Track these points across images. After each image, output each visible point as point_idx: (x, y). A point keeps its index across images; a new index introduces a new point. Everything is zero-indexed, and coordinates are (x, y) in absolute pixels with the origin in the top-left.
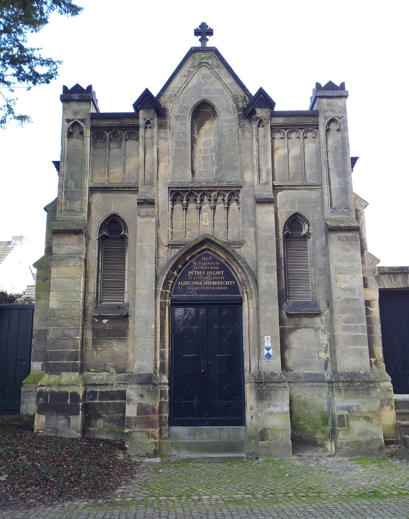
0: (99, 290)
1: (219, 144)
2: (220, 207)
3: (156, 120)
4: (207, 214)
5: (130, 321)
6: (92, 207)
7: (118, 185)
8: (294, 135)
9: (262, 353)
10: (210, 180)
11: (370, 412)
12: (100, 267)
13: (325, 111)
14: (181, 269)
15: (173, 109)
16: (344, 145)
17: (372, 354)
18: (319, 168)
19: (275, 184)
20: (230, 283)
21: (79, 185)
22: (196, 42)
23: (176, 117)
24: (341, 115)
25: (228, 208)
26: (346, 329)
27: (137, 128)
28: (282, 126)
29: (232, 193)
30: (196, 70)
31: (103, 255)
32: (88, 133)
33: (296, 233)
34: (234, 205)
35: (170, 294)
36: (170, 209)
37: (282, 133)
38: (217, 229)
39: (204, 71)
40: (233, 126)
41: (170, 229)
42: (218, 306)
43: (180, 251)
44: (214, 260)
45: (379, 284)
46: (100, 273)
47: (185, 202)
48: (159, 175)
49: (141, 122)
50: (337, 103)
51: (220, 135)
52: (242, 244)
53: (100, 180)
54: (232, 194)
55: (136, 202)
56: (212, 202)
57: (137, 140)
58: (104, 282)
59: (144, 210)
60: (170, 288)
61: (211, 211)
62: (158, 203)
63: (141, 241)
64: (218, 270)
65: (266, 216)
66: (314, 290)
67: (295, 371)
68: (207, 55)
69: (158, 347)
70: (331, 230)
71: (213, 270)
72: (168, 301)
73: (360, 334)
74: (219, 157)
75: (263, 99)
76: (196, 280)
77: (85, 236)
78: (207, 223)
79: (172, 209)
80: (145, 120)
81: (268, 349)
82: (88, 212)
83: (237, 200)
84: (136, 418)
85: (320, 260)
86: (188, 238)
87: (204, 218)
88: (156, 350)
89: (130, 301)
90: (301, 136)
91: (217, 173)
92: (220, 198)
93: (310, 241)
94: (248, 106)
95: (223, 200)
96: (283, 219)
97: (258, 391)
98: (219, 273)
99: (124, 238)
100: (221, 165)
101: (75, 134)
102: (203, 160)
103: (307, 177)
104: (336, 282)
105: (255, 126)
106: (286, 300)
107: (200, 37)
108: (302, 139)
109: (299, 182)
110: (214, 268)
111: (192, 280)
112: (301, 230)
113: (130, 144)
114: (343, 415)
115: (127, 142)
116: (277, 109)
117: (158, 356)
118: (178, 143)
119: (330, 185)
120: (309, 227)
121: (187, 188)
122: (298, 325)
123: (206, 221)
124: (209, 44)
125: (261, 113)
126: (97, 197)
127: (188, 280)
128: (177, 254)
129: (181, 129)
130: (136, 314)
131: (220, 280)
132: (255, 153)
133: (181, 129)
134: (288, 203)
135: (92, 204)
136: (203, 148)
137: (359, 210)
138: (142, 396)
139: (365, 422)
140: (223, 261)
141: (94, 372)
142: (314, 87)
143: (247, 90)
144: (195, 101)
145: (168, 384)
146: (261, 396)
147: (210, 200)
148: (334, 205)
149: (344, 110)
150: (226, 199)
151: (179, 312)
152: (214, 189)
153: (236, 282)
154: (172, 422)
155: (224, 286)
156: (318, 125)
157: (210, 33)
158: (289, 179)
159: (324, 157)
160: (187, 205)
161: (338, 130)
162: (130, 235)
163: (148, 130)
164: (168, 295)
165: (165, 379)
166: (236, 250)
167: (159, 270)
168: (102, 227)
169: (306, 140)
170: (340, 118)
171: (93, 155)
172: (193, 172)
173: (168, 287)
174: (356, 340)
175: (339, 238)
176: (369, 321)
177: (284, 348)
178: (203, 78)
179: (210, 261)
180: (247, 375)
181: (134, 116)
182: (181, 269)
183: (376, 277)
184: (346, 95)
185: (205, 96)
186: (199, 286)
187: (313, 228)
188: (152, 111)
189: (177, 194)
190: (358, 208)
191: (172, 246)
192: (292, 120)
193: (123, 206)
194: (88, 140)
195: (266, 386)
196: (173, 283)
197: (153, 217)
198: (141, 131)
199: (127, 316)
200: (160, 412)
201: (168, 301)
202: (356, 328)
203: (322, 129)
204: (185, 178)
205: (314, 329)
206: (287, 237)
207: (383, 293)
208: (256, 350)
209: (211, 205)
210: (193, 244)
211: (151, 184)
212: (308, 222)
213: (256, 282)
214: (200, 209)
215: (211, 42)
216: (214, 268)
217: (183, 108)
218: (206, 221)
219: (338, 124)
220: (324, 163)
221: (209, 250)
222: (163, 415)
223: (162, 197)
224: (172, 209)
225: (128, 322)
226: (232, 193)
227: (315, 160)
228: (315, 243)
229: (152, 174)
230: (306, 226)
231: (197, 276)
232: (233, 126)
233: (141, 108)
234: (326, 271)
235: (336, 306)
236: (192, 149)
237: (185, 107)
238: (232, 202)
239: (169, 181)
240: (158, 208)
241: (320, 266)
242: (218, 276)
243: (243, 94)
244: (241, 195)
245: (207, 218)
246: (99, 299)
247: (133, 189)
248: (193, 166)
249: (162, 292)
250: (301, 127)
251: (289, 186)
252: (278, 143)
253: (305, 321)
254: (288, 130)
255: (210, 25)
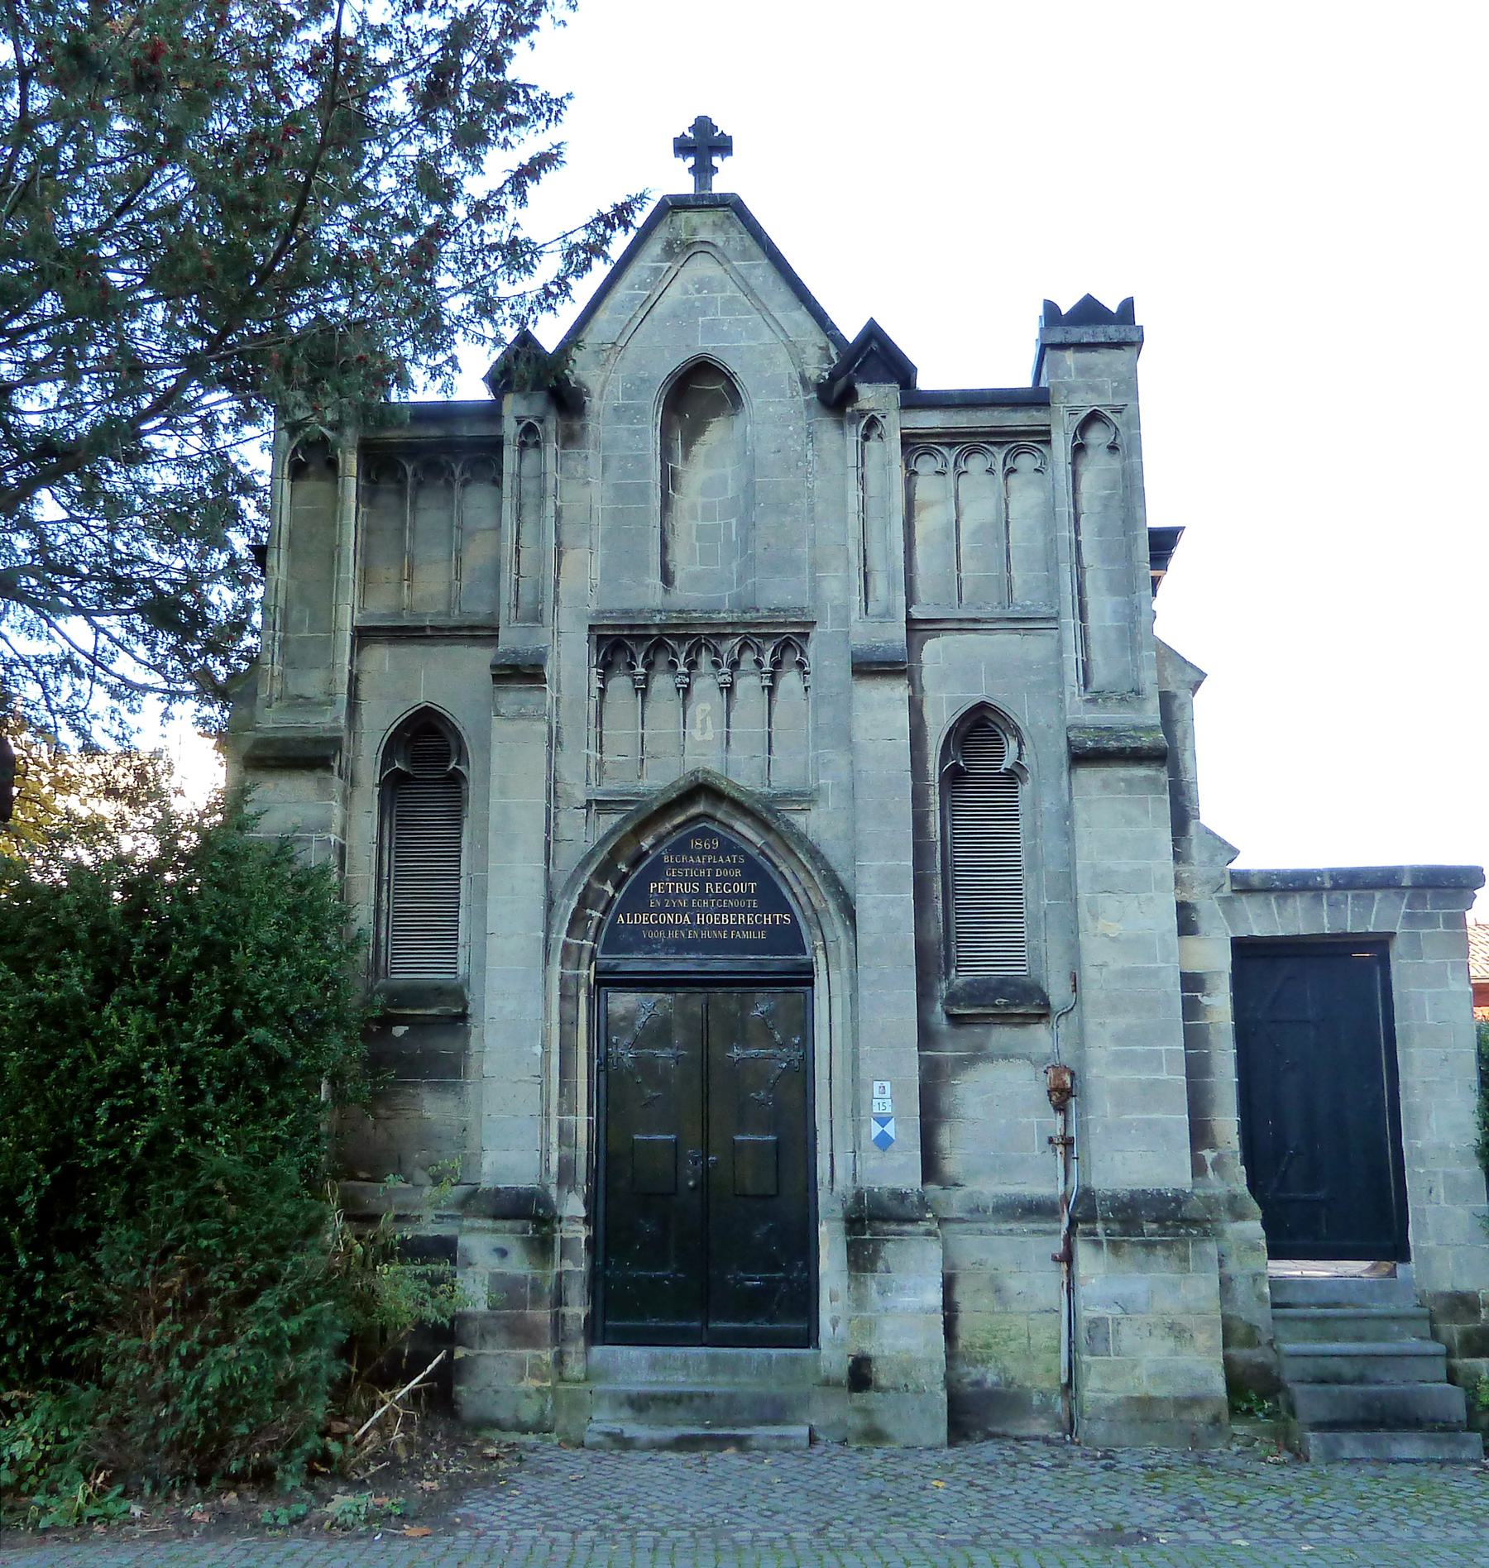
0: (383, 936)
1: (749, 489)
2: (749, 684)
3: (552, 425)
4: (708, 707)
5: (474, 1031)
7: (439, 622)
8: (976, 464)
9: (864, 1131)
10: (721, 599)
12: (386, 869)
13: (1071, 390)
14: (626, 876)
17: (1200, 1133)
18: (1051, 564)
19: (916, 616)
20: (774, 920)
21: (325, 621)
22: (679, 179)
23: (616, 409)
24: (1118, 402)
25: (771, 690)
28: (938, 435)
29: (783, 642)
30: (678, 266)
31: (394, 831)
32: (350, 463)
33: (981, 765)
34: (790, 680)
35: (593, 951)
36: (595, 693)
37: (939, 458)
39: (703, 267)
40: (791, 436)
41: (593, 753)
42: (740, 989)
43: (625, 820)
44: (728, 848)
45: (1233, 927)
46: (385, 887)
47: (641, 670)
48: (561, 589)
49: (510, 429)
51: (750, 464)
53: (381, 607)
54: (786, 645)
55: (487, 674)
56: (724, 669)
57: (497, 483)
59: (512, 698)
60: (591, 933)
61: (720, 700)
62: (558, 674)
63: (503, 793)
66: (1034, 942)
67: (971, 1187)
68: (709, 217)
70: (1080, 757)
71: (723, 880)
72: (587, 973)
73: (1164, 1076)
74: (748, 527)
75: (877, 355)
76: (672, 910)
77: (340, 776)
78: (709, 736)
79: (602, 691)
80: (519, 423)
81: (883, 1121)
82: (349, 703)
83: (801, 664)
84: (486, 1316)
85: (1051, 844)
87: (699, 718)
88: (548, 1121)
89: (473, 974)
90: (998, 467)
91: (741, 580)
92: (749, 657)
93: (1025, 790)
94: (833, 377)
95: (759, 663)
97: (850, 1246)
98: (740, 888)
101: (311, 468)
102: (698, 539)
103: (1016, 594)
106: (947, 974)
107: (691, 161)
108: (1000, 474)
110: (727, 873)
111: (662, 910)
113: (477, 498)
114: (1104, 1320)
115: (469, 489)
117: (554, 1138)
118: (621, 492)
119: (1083, 618)
120: (1020, 746)
121: (645, 626)
123: (703, 730)
125: (872, 395)
126: (379, 657)
127: (650, 911)
128: (612, 832)
129: (630, 448)
131: (745, 911)
133: (630, 448)
134: (953, 676)
135: (364, 678)
136: (700, 500)
137: (1175, 696)
138: (503, 1253)
139: (1170, 1343)
140: (754, 852)
141: (367, 1180)
142: (1040, 311)
143: (833, 327)
144: (671, 361)
145: (586, 1220)
146: (861, 1259)
147: (716, 664)
148: (1099, 678)
149: (1129, 385)
150: (767, 659)
151: (622, 1002)
152: (729, 630)
154: (596, 1332)
155: (755, 928)
156: (1048, 433)
157: (724, 146)
158: (960, 599)
159: (1067, 533)
160: (646, 681)
161: (1113, 448)
162: (472, 773)
163: (531, 454)
164: (586, 956)
165: (574, 1206)
166: (796, 817)
167: (560, 882)
170: (1118, 411)
171: (368, 530)
172: (667, 577)
173: (587, 932)
174: (1151, 1093)
175: (1106, 785)
176: (1194, 1037)
177: (931, 1115)
178: (699, 291)
179: (717, 853)
180: (823, 1196)
181: (490, 413)
182: (626, 876)
183: (1226, 900)
184: (1136, 339)
186: (681, 927)
187: (1037, 744)
189: (622, 646)
190: (1171, 688)
196: (601, 920)
197: (540, 718)
198: (509, 455)
199: (463, 1017)
200: (559, 1300)
201: (585, 972)
202: (1152, 1060)
203: (1061, 444)
204: (646, 596)
205: (1029, 1059)
206: (954, 778)
207: (1245, 950)
208: (849, 1123)
209: (720, 679)
210: (663, 800)
211: (537, 617)
212: (1017, 732)
214: (687, 691)
215: (726, 178)
216: (727, 873)
217: (638, 382)
218: (703, 730)
219: (1113, 429)
221: (712, 818)
222: (569, 1311)
223: (570, 658)
224: (602, 691)
225: (468, 1034)
226: (783, 642)
228: (1036, 799)
231: (676, 897)
232: (791, 436)
233: (508, 387)
237: (643, 380)
238: (785, 669)
240: (558, 691)
241: (1051, 868)
242: (739, 896)
243: (820, 339)
244: (811, 649)
245: (709, 723)
246: (383, 963)
247: (483, 633)
248: (669, 558)
249: (566, 946)
251: (960, 620)
252: (928, 487)
254: (957, 449)
255: (724, 125)
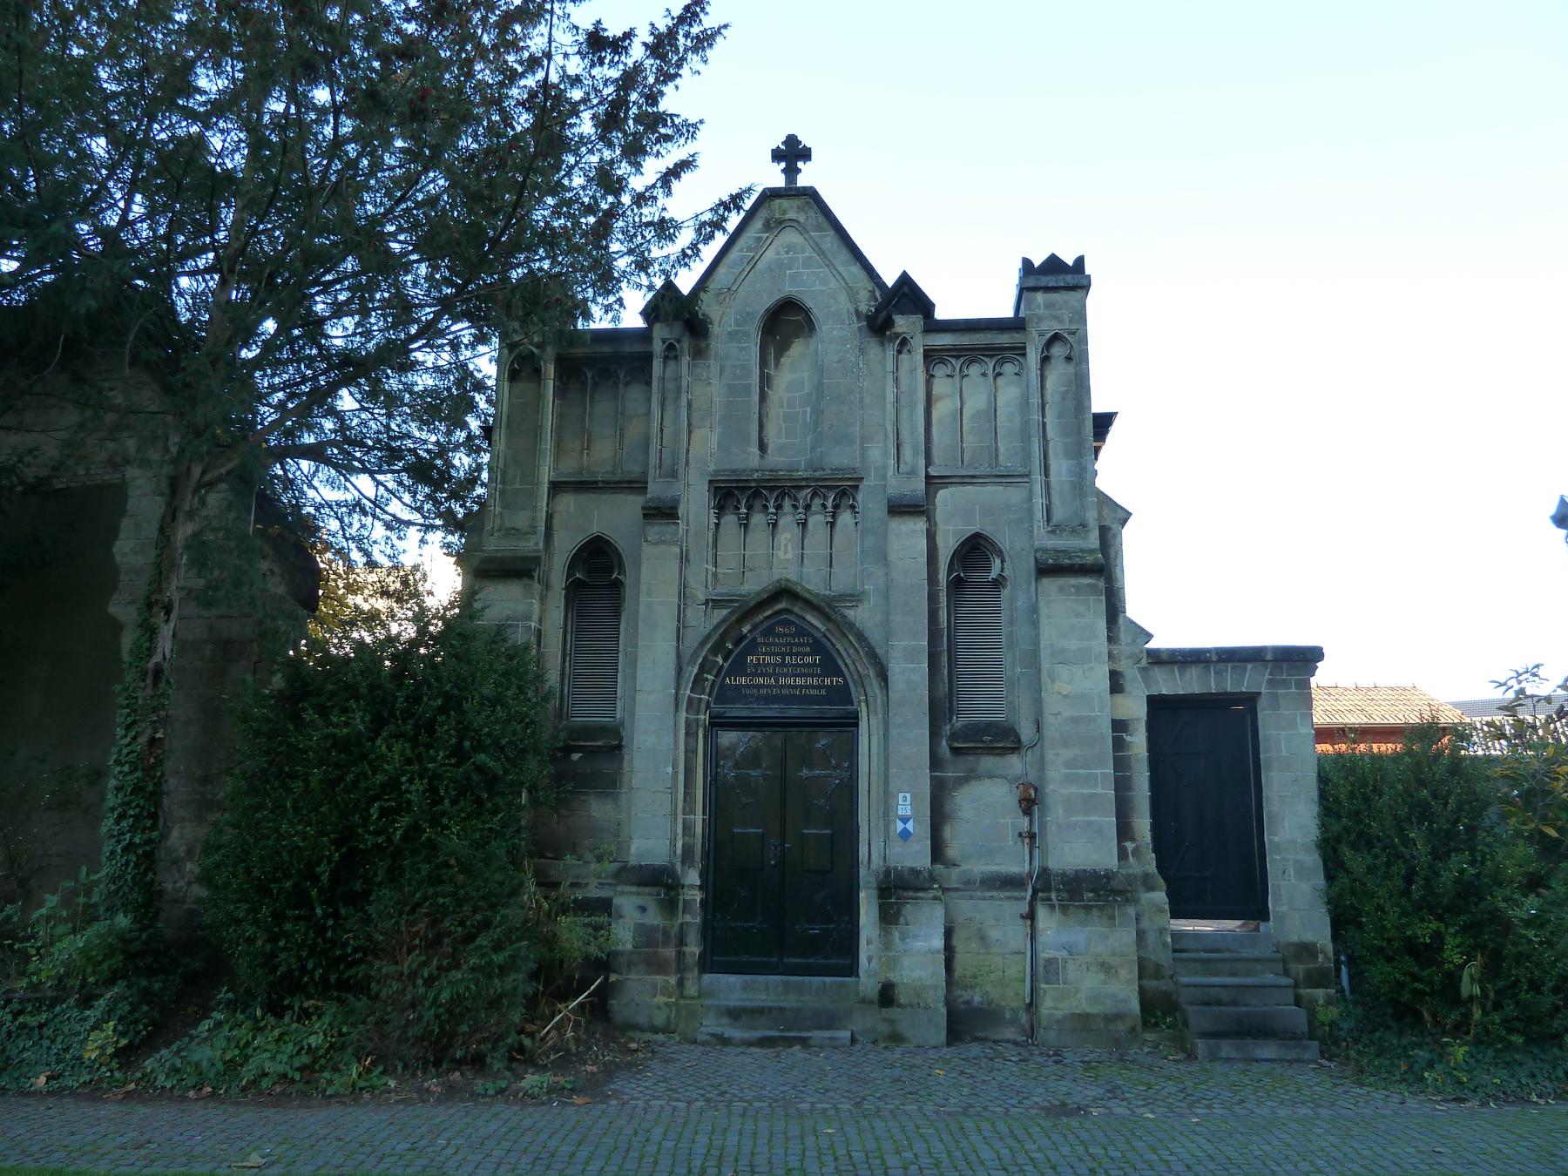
1: (819, 388)
2: (817, 520)
6: (556, 522)
7: (608, 477)
8: (975, 370)
9: (892, 827)
11: (1114, 954)
13: (1040, 319)
14: (731, 651)
15: (720, 315)
16: (1080, 386)
17: (1124, 831)
18: (1025, 437)
22: (774, 177)
24: (1073, 327)
25: (832, 524)
26: (1070, 780)
27: (648, 358)
29: (841, 491)
32: (550, 370)
33: (975, 576)
34: (845, 518)
35: (708, 703)
36: (712, 526)
38: (809, 568)
39: (790, 237)
44: (801, 632)
45: (1147, 685)
49: (658, 347)
50: (1066, 302)
51: (820, 370)
52: (860, 601)
53: (568, 468)
55: (639, 512)
57: (648, 384)
58: (577, 676)
59: (655, 530)
61: (797, 531)
64: (808, 654)
65: (908, 537)
67: (964, 867)
68: (795, 203)
69: (680, 811)
71: (797, 654)
72: (704, 717)
73: (1099, 791)
74: (818, 413)
75: (908, 296)
76: (762, 675)
78: (790, 555)
81: (905, 820)
83: (853, 507)
86: (745, 589)
90: (990, 371)
91: (813, 450)
92: (817, 502)
93: (1005, 593)
96: (947, 545)
97: (881, 907)
98: (809, 660)
99: (617, 586)
100: (821, 434)
104: (1053, 681)
105: (891, 351)
107: (783, 165)
108: (991, 378)
109: (984, 469)
112: (989, 569)
113: (634, 394)
114: (1056, 959)
116: (940, 314)
117: (680, 831)
119: (1047, 474)
122: (972, 771)
124: (802, 181)
126: (567, 502)
130: (635, 745)
131: (812, 676)
132: (890, 408)
134: (957, 513)
138: (643, 909)
140: (819, 635)
142: (1020, 265)
144: (768, 301)
145: (701, 888)
146: (889, 916)
147: (795, 507)
150: (830, 503)
151: (727, 738)
153: (845, 680)
155: (819, 687)
157: (806, 154)
161: (1069, 359)
162: (628, 581)
164: (703, 706)
165: (693, 877)
168: (574, 563)
169: (1000, 380)
171: (560, 417)
175: (1061, 590)
176: (1121, 764)
177: (939, 817)
180: (863, 872)
182: (731, 651)
185: (789, 290)
186: (768, 686)
187: (1014, 563)
188: (678, 328)
189: (733, 494)
191: (716, 603)
192: (965, 340)
193: (613, 517)
194: (550, 385)
195: (898, 890)
197: (675, 543)
198: (657, 365)
199: (619, 747)
200: (681, 942)
203: (1033, 356)
204: (749, 460)
206: (957, 585)
207: (1155, 703)
210: (757, 600)
211: (673, 474)
212: (1000, 553)
213: (883, 675)
214: (775, 525)
220: (1035, 431)
223: (696, 502)
224: (717, 525)
226: (841, 491)
227: (1018, 421)
228: (1014, 598)
229: (675, 455)
230: (998, 562)
231: (766, 665)
234: (1033, 659)
235: (1050, 732)
236: (763, 397)
239: (712, 467)
243: (869, 285)
244: (860, 497)
247: (637, 485)
250: (989, 351)
252: (941, 386)
253: (987, 762)
255: (806, 140)
